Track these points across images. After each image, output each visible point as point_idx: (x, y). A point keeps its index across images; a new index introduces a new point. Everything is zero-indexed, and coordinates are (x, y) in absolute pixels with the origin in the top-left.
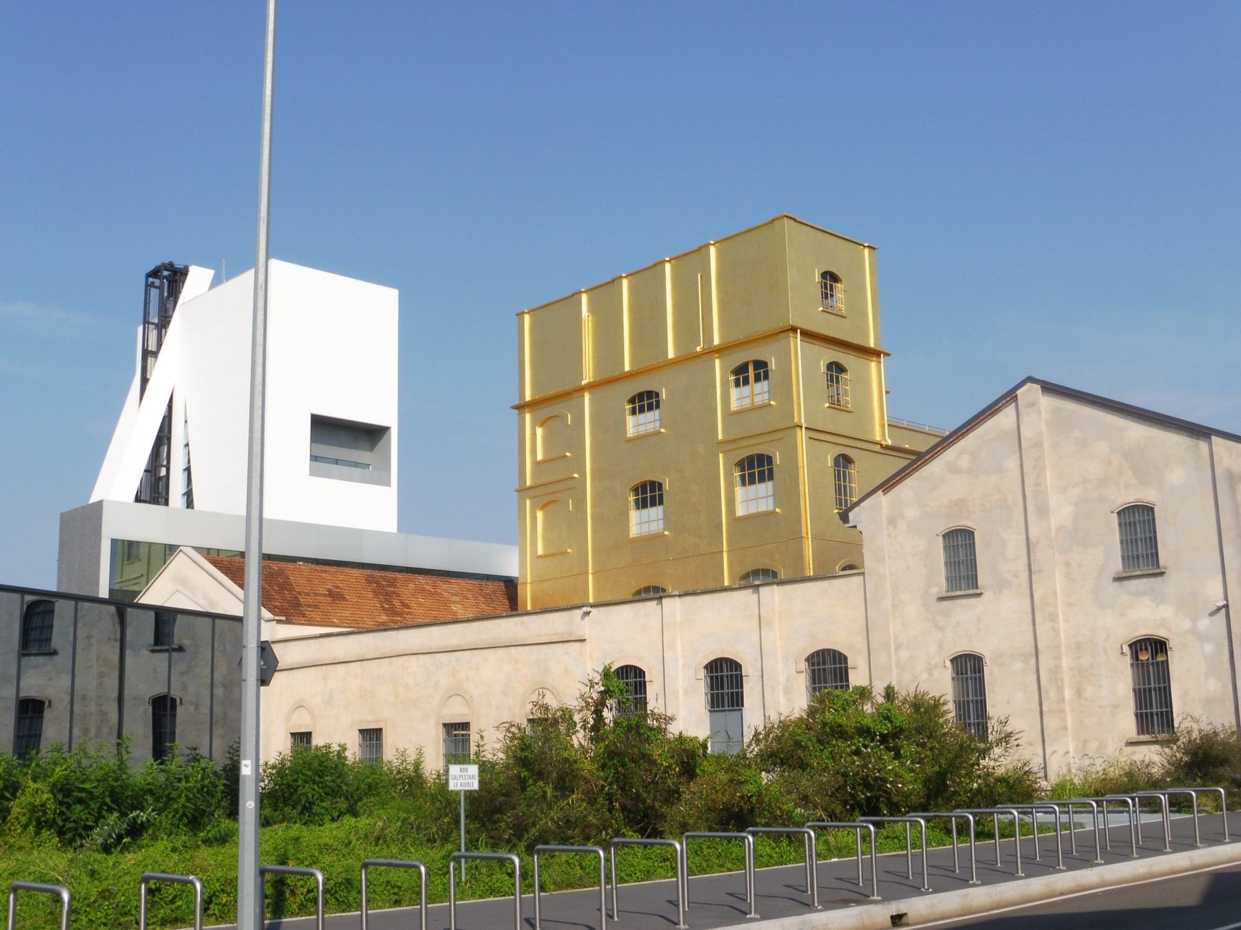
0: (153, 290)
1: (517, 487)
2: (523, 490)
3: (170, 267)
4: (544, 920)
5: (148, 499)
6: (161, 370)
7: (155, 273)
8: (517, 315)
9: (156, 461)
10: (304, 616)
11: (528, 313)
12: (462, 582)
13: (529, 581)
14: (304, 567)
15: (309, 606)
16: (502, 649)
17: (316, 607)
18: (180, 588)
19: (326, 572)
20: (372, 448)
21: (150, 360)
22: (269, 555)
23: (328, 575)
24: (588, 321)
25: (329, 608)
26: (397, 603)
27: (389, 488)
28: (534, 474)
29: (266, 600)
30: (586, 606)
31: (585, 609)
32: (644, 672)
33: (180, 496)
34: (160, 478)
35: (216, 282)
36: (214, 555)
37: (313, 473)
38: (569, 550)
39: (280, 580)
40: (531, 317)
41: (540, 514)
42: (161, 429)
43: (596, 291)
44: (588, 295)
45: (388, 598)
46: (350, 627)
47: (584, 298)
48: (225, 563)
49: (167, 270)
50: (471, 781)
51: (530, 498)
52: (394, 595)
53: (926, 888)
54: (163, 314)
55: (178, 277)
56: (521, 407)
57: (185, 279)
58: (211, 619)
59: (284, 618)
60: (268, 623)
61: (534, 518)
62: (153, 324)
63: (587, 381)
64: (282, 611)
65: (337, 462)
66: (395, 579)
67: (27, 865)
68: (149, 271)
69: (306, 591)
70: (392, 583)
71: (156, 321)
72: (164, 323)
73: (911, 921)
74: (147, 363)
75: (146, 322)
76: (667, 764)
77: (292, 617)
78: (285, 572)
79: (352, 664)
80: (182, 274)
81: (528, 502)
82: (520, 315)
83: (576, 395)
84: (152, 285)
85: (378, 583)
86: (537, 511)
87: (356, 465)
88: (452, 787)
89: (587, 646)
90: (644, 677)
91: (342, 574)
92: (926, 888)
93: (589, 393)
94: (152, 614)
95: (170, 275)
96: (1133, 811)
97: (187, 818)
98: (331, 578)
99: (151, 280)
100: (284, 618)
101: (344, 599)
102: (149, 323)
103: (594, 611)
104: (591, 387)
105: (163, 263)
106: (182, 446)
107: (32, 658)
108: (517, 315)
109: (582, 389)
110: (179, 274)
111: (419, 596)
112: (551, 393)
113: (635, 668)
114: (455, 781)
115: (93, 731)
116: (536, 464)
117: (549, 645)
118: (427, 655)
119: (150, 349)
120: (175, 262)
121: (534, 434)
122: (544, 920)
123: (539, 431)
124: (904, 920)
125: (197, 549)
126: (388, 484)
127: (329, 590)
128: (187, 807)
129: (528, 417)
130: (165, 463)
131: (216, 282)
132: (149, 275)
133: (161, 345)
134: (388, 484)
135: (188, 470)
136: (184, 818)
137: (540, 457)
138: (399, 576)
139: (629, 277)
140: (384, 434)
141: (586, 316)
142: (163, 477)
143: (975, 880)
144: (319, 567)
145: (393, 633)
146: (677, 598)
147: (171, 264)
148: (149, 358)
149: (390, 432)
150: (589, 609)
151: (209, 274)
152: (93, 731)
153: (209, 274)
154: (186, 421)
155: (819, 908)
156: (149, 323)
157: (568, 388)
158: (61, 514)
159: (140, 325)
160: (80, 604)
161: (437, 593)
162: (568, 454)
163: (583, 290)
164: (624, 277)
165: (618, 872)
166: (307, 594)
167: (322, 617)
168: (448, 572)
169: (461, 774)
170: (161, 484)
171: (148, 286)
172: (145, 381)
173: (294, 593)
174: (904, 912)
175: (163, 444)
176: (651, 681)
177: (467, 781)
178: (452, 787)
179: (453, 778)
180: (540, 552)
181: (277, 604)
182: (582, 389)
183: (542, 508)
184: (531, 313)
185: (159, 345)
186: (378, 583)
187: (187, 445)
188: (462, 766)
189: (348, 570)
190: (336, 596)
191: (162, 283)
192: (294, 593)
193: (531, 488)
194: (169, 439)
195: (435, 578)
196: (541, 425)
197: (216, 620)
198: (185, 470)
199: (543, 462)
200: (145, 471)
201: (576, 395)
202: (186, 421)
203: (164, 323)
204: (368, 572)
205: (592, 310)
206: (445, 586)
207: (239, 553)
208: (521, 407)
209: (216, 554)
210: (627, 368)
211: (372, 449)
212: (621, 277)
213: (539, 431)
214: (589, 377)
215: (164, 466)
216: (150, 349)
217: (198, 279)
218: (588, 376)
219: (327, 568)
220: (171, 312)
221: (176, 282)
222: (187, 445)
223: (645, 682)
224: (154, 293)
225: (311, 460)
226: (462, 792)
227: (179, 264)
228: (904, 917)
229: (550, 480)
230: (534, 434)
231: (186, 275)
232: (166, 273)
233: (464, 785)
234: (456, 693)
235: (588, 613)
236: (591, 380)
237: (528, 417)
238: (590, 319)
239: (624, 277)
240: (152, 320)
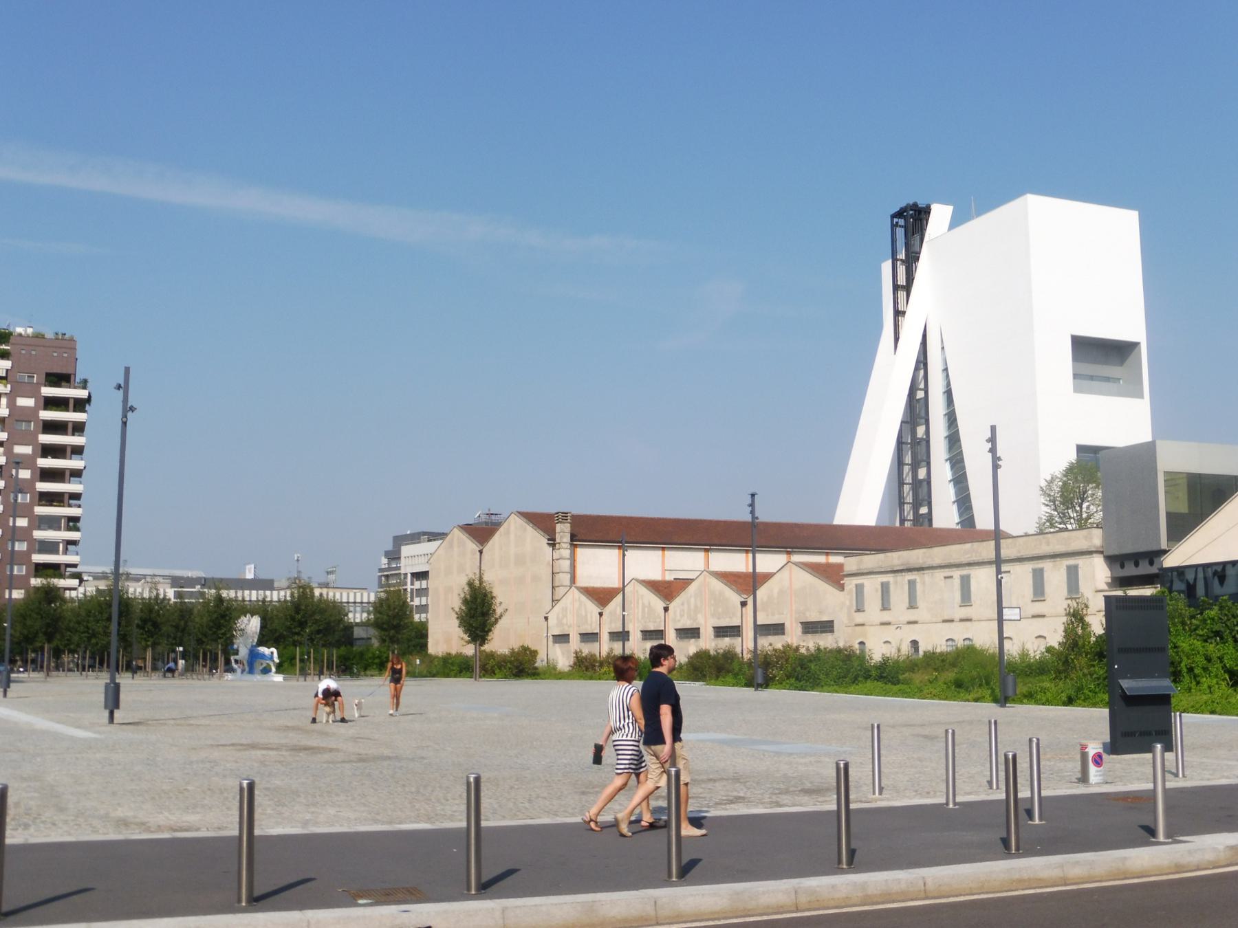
3: (915, 207)
7: (899, 214)
20: (1121, 363)
21: (1068, 882)
22: (962, 460)
27: (1142, 400)
29: (31, 644)
37: (1077, 389)
49: (912, 210)
55: (923, 216)
57: (929, 216)
67: (909, 690)
68: (894, 212)
75: (895, 260)
80: (925, 212)
96: (69, 529)
99: (896, 220)
102: (897, 260)
105: (908, 204)
110: (923, 213)
126: (1141, 396)
132: (893, 216)
134: (1141, 396)
135: (949, 393)
140: (1135, 348)
142: (921, 399)
154: (943, 348)
159: (885, 260)
171: (894, 226)
198: (944, 370)
202: (943, 348)
215: (921, 390)
217: (940, 215)
221: (921, 220)
224: (900, 233)
225: (1074, 378)
231: (929, 213)
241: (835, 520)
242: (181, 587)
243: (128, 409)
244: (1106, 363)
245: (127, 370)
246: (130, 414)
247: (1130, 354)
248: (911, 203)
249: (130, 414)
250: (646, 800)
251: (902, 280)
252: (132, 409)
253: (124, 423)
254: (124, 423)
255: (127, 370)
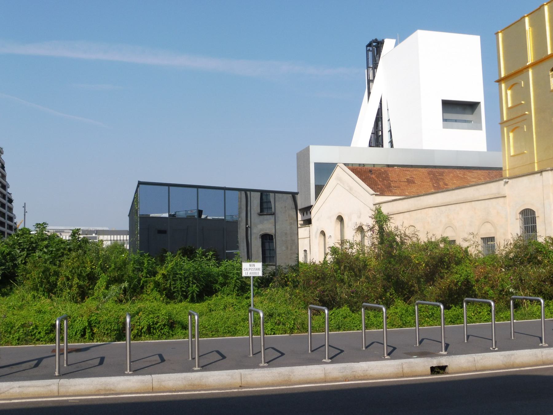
0: (369, 52)
1: (500, 121)
2: (503, 123)
3: (376, 41)
4: (439, 342)
5: (374, 146)
6: (375, 87)
7: (370, 45)
8: (495, 34)
9: (377, 129)
10: (391, 191)
11: (501, 32)
12: (479, 172)
13: (507, 169)
14: (397, 169)
15: (395, 187)
16: (469, 203)
17: (399, 187)
18: (339, 182)
19: (408, 171)
20: (472, 113)
22: (388, 165)
23: (409, 172)
24: (529, 31)
25: (405, 187)
26: (441, 183)
28: (508, 114)
30: (506, 179)
31: (505, 180)
32: (535, 212)
33: (388, 143)
34: (379, 136)
35: (396, 44)
36: (350, 166)
37: (444, 127)
38: (525, 152)
39: (384, 176)
40: (503, 34)
41: (511, 135)
42: (378, 114)
43: (533, 14)
44: (529, 17)
45: (438, 181)
46: (402, 196)
47: (527, 20)
48: (358, 170)
49: (374, 42)
50: (257, 271)
51: (506, 127)
52: (441, 180)
53: (494, 347)
54: (374, 62)
56: (500, 81)
58: (223, 191)
59: (379, 193)
60: (372, 196)
61: (508, 137)
62: (371, 68)
63: (530, 63)
64: (381, 190)
65: (456, 121)
66: (443, 172)
69: (395, 180)
70: (441, 174)
71: (372, 66)
72: (375, 66)
73: (449, 371)
74: (370, 85)
75: (368, 67)
76: (417, 262)
77: (385, 193)
78: (387, 172)
79: (406, 213)
81: (505, 129)
82: (497, 33)
83: (526, 71)
84: (369, 50)
85: (434, 175)
86: (510, 133)
87: (465, 121)
88: (244, 274)
89: (507, 200)
90: (535, 215)
91: (415, 171)
92: (494, 347)
93: (532, 69)
94: (259, 194)
95: (376, 45)
97: (237, 287)
98: (409, 174)
99: (368, 48)
100: (379, 193)
101: (414, 183)
102: (369, 67)
103: (510, 181)
104: (533, 65)
106: (387, 121)
107: (265, 216)
108: (495, 34)
109: (528, 67)
110: (380, 44)
111: (454, 179)
112: (513, 72)
113: (531, 210)
114: (247, 271)
115: (289, 248)
116: (508, 109)
117: (490, 200)
118: (436, 208)
119: (370, 79)
120: (378, 39)
121: (506, 94)
122: (439, 342)
123: (509, 92)
124: (447, 370)
125: (345, 164)
126: (480, 129)
127: (408, 179)
128: (237, 282)
129: (503, 86)
130: (381, 129)
131: (396, 44)
132: (367, 46)
133: (375, 77)
134: (480, 129)
135: (390, 131)
136: (236, 287)
137: (510, 105)
138: (446, 170)
139: (548, 4)
141: (528, 28)
143: (544, 343)
144: (404, 169)
145: (422, 198)
146: (550, 172)
147: (376, 40)
148: (371, 83)
149: (480, 106)
150: (507, 180)
151: (394, 41)
152: (289, 248)
153: (394, 41)
154: (388, 109)
155: (496, 349)
156: (369, 67)
157: (520, 67)
158: (297, 154)
160: (170, 187)
161: (464, 178)
162: (523, 102)
163: (526, 15)
164: (546, 4)
165: (548, 317)
166: (396, 182)
167: (401, 192)
168: (479, 167)
169: (250, 267)
170: (380, 138)
171: (368, 51)
172: (369, 93)
173: (389, 181)
174: (445, 364)
175: (379, 121)
176: (538, 217)
177: (254, 271)
178: (244, 274)
179: (245, 269)
180: (512, 153)
181: (380, 187)
182: (528, 67)
183: (513, 131)
184: (502, 32)
185: (374, 77)
186: (434, 175)
187: (389, 120)
188: (251, 263)
189: (420, 169)
190: (410, 182)
191: (373, 49)
192: (389, 181)
193: (507, 121)
194: (382, 118)
195: (465, 171)
196: (510, 89)
197: (252, 192)
198: (389, 131)
199: (511, 108)
200: (372, 133)
201: (525, 71)
202: (388, 109)
203: (375, 66)
204: (430, 169)
205: (531, 25)
206: (470, 174)
207: (384, 165)
208: (500, 81)
209: (373, 166)
210: (549, 52)
211: (472, 113)
212: (544, 5)
213: (509, 92)
214: (531, 60)
216: (370, 79)
217: (389, 44)
218: (531, 59)
219: (409, 169)
220: (378, 62)
221: (379, 47)
222: (389, 120)
223: (535, 217)
224: (370, 54)
226: (252, 277)
227: (379, 39)
228: (447, 368)
229: (515, 116)
230: (506, 94)
231: (383, 43)
232: (374, 44)
233: (253, 273)
234: (449, 226)
235: (507, 182)
236: (533, 61)
237: (503, 86)
238: (531, 30)
239: (546, 4)
240: (370, 66)
241: (127, 229)
242: (86, 235)
243: (25, 212)
244: (464, 113)
245: (25, 203)
246: (24, 206)
247: (476, 108)
248: (374, 39)
249: (24, 206)
250: (340, 351)
251: (371, 78)
252: (27, 212)
253: (25, 215)
254: (25, 215)
255: (25, 203)
